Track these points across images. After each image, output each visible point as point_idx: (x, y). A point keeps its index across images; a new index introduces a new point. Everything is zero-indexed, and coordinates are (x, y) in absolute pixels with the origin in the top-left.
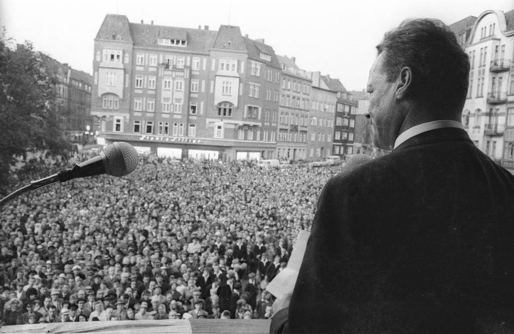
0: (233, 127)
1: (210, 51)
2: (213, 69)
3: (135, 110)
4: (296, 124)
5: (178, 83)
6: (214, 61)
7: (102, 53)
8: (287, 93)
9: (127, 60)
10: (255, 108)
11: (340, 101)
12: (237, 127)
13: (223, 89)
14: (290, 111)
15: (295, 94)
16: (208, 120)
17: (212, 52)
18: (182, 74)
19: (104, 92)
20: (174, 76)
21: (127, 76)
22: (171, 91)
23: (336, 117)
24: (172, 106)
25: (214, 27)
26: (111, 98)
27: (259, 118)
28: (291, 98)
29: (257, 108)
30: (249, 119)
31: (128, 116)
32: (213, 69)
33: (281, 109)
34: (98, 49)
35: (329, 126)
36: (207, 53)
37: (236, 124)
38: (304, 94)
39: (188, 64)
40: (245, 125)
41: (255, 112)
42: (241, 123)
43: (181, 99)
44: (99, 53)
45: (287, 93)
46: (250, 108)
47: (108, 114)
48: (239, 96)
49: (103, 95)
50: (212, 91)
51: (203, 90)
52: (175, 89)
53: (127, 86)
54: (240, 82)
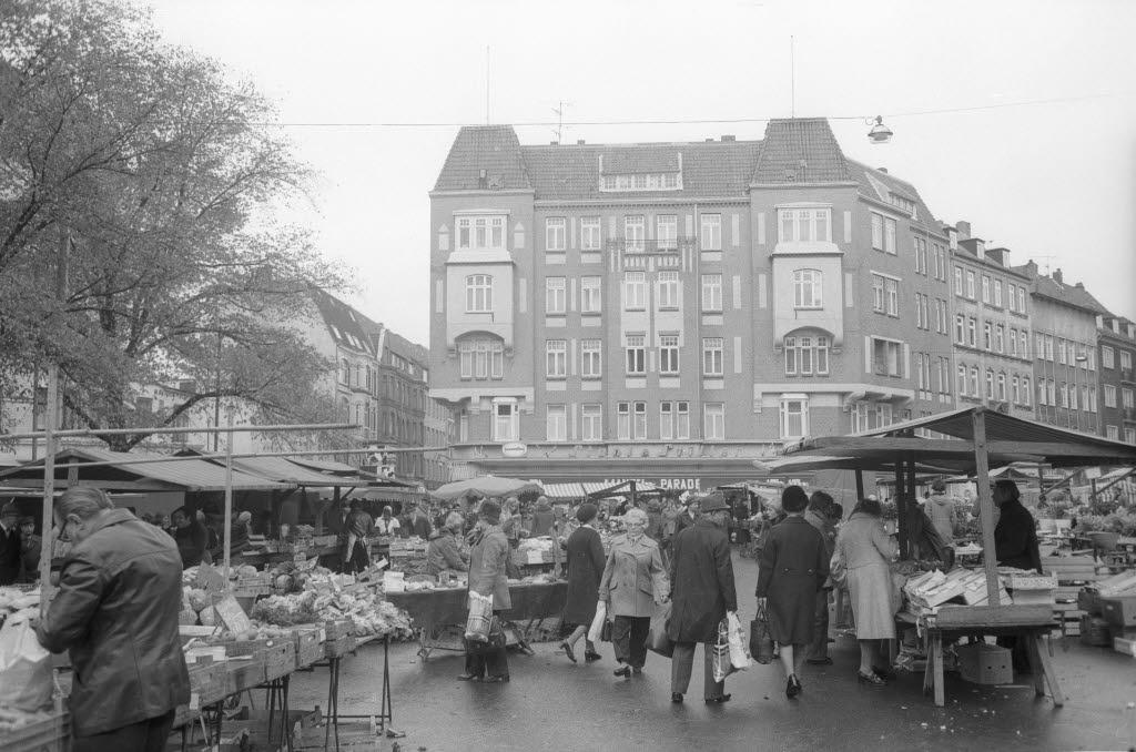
0: (834, 402)
1: (748, 192)
2: (762, 240)
3: (548, 249)
4: (1004, 400)
5: (663, 287)
6: (761, 217)
7: (452, 228)
8: (969, 309)
9: (520, 240)
10: (891, 344)
11: (1104, 340)
12: (847, 400)
13: (798, 294)
14: (982, 360)
15: (990, 313)
16: (760, 388)
17: (753, 193)
18: (672, 261)
19: (457, 334)
20: (652, 269)
21: (523, 282)
22: (648, 311)
23: (1101, 384)
24: (652, 353)
25: (756, 133)
26: (488, 346)
27: (907, 375)
28: (981, 324)
29: (897, 344)
30: (882, 375)
31: (529, 393)
32: (762, 240)
33: (958, 356)
34: (441, 221)
35: (1086, 408)
36: (744, 198)
37: (843, 395)
38: (1014, 314)
39: (689, 234)
40: (868, 397)
41: (892, 356)
42: (860, 389)
43: (676, 334)
44: (444, 228)
45: (969, 309)
46: (879, 344)
47: (475, 393)
48: (845, 309)
49: (465, 337)
50: (763, 304)
51: (737, 304)
52: (657, 306)
53: (523, 307)
54: (845, 270)
